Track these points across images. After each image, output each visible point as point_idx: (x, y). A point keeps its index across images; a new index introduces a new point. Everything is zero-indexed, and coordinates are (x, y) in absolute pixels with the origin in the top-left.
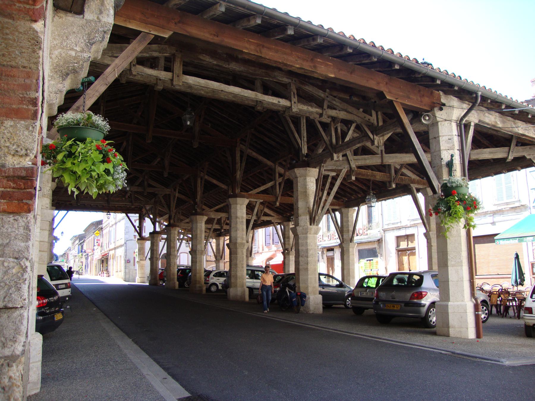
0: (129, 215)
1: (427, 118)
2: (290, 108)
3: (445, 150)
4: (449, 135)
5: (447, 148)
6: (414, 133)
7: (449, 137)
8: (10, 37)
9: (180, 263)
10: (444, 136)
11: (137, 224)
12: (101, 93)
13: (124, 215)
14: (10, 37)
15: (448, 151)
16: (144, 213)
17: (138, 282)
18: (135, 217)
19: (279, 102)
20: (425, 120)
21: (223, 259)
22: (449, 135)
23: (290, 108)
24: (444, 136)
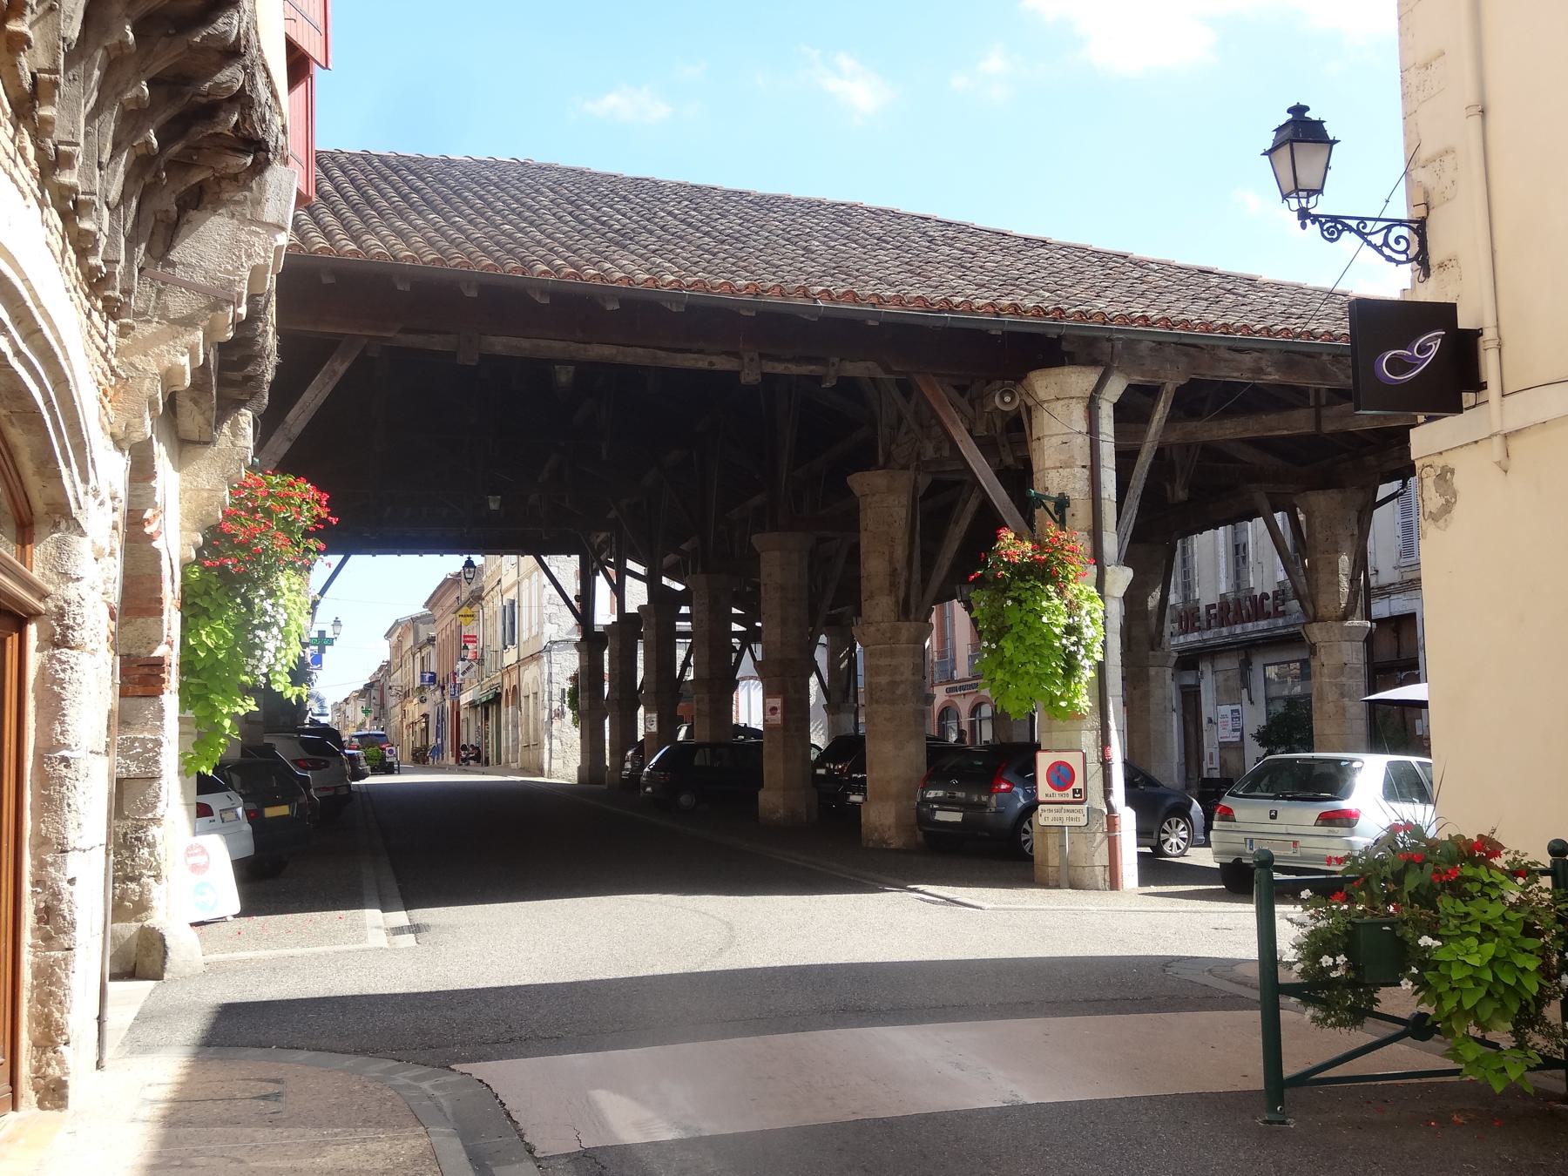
0: (545, 559)
1: (1007, 399)
2: (737, 373)
3: (1053, 468)
4: (1063, 434)
5: (1058, 464)
6: (966, 432)
7: (1065, 438)
8: (137, 555)
9: (1046, 751)
10: (1052, 436)
11: (572, 587)
12: (282, 456)
13: (529, 560)
14: (137, 555)
15: (1060, 470)
16: (684, 547)
17: (1254, 909)
18: (567, 567)
19: (711, 363)
20: (1002, 398)
21: (851, 699)
22: (1063, 434)
23: (737, 373)
24: (1052, 436)
